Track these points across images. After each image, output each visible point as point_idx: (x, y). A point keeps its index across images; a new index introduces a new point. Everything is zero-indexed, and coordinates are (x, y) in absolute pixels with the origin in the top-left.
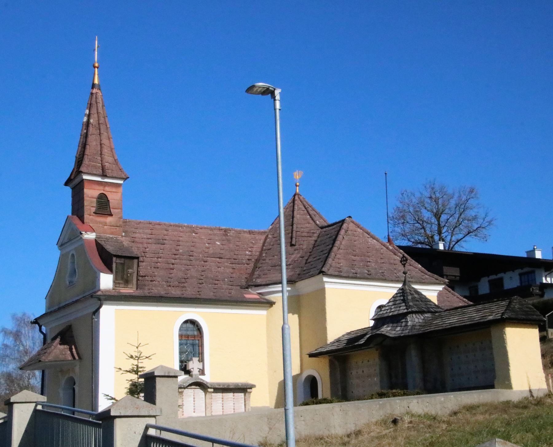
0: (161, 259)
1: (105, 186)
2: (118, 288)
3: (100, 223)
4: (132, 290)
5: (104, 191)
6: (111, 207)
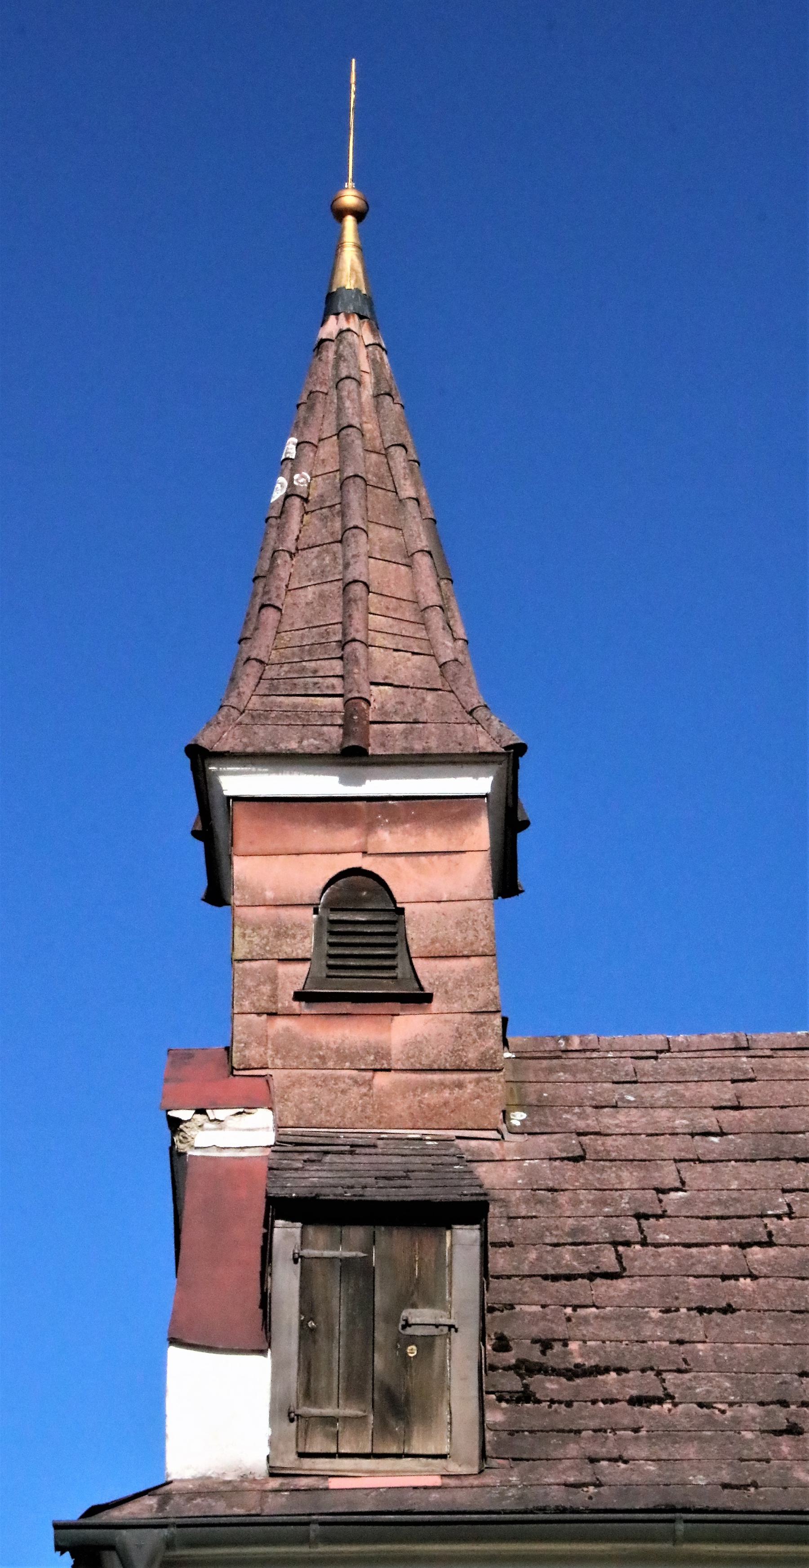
0: (772, 1251)
1: (370, 827)
2: (322, 1464)
3: (344, 1056)
4: (431, 1473)
5: (365, 853)
6: (414, 949)
